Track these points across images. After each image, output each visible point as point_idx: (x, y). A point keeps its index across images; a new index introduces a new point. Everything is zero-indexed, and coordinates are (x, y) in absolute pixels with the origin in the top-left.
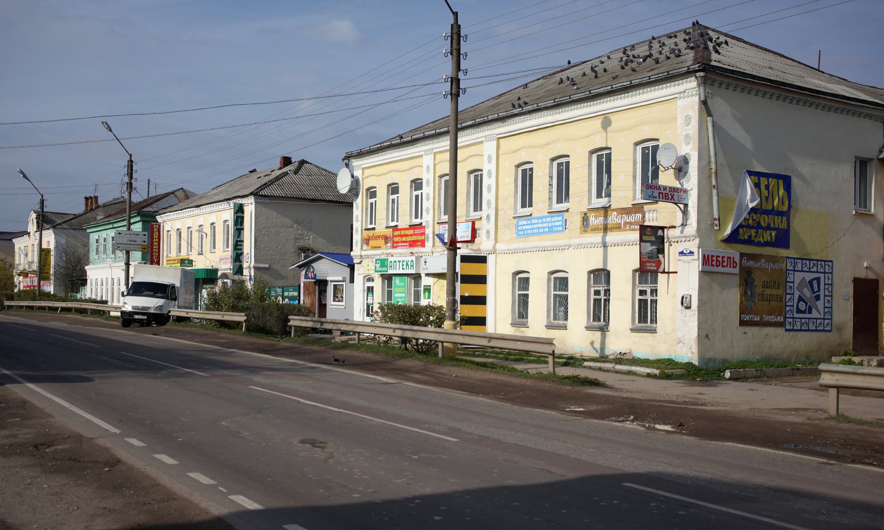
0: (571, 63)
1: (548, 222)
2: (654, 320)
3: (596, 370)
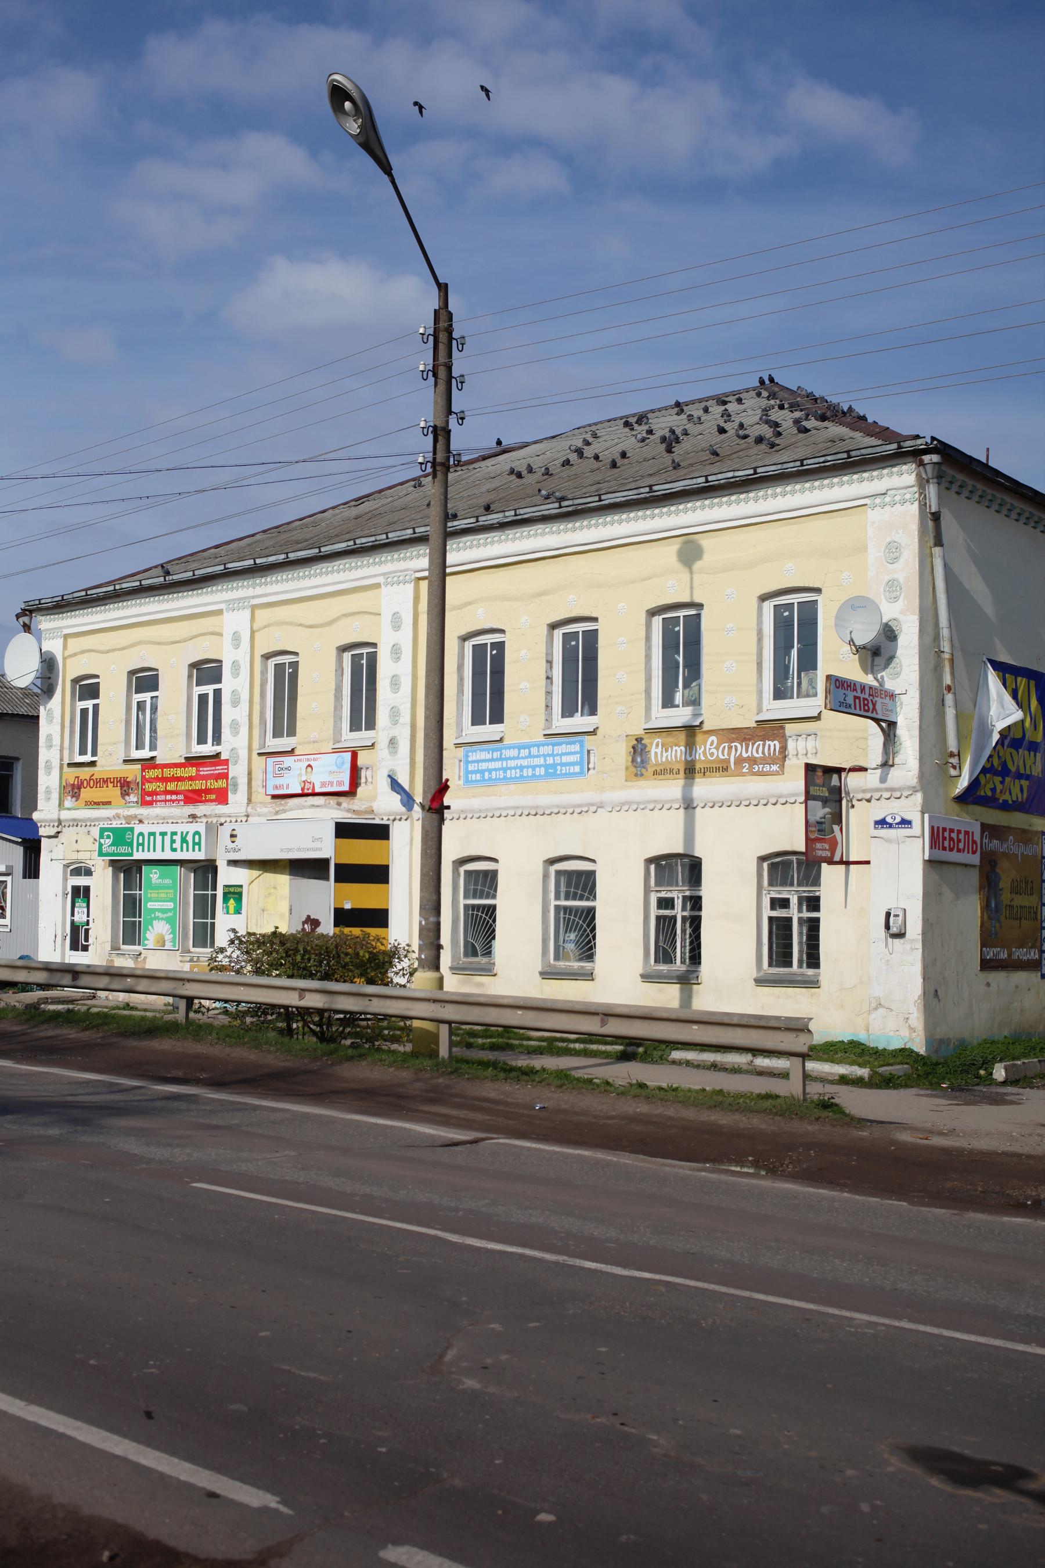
0: (504, 444)
1: (545, 756)
2: (813, 959)
3: (704, 1067)
